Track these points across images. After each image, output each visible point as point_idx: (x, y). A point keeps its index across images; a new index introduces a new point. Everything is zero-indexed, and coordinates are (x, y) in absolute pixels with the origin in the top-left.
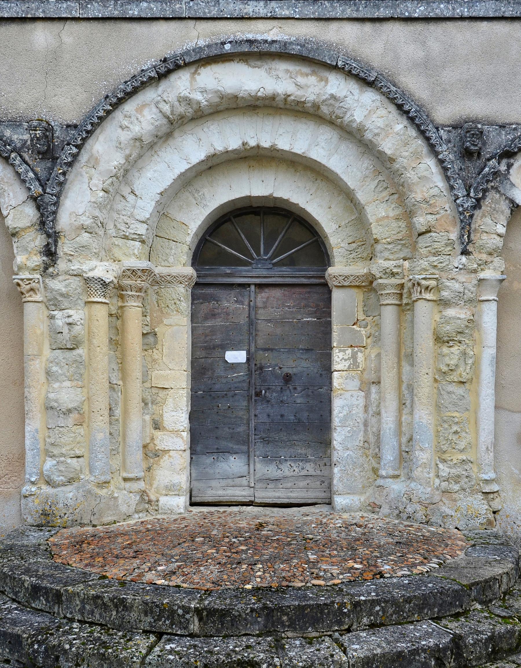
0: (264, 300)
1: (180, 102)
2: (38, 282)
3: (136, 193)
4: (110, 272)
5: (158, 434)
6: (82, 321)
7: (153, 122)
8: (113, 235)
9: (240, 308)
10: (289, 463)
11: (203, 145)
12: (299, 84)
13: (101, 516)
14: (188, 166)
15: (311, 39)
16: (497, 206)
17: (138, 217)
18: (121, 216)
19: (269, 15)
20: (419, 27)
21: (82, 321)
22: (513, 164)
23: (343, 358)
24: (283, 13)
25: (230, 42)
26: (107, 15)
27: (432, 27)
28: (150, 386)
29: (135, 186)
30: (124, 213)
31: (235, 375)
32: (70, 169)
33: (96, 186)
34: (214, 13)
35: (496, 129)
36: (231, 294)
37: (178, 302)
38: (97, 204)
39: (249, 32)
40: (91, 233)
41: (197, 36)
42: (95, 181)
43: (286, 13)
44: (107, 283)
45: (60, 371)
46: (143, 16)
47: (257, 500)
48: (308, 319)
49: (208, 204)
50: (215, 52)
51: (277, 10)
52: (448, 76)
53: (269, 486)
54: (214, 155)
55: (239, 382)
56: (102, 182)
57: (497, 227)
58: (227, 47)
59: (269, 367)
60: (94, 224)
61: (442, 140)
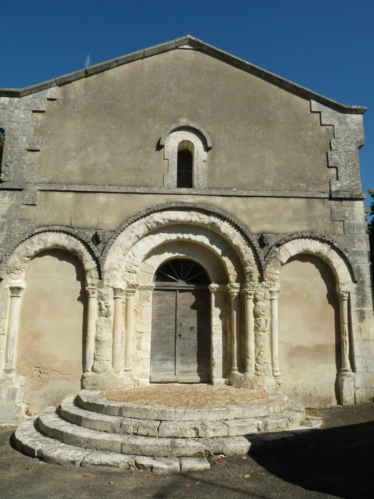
1: (154, 223)
5: (139, 352)
10: (192, 365)
13: (116, 386)
17: (135, 264)
19: (189, 193)
20: (245, 198)
22: (281, 248)
26: (127, 191)
27: (249, 199)
30: (129, 262)
34: (168, 192)
39: (181, 199)
42: (120, 251)
43: (195, 192)
46: (141, 192)
47: (179, 381)
50: (168, 206)
52: (256, 216)
53: (184, 375)
55: (172, 330)
58: (173, 204)
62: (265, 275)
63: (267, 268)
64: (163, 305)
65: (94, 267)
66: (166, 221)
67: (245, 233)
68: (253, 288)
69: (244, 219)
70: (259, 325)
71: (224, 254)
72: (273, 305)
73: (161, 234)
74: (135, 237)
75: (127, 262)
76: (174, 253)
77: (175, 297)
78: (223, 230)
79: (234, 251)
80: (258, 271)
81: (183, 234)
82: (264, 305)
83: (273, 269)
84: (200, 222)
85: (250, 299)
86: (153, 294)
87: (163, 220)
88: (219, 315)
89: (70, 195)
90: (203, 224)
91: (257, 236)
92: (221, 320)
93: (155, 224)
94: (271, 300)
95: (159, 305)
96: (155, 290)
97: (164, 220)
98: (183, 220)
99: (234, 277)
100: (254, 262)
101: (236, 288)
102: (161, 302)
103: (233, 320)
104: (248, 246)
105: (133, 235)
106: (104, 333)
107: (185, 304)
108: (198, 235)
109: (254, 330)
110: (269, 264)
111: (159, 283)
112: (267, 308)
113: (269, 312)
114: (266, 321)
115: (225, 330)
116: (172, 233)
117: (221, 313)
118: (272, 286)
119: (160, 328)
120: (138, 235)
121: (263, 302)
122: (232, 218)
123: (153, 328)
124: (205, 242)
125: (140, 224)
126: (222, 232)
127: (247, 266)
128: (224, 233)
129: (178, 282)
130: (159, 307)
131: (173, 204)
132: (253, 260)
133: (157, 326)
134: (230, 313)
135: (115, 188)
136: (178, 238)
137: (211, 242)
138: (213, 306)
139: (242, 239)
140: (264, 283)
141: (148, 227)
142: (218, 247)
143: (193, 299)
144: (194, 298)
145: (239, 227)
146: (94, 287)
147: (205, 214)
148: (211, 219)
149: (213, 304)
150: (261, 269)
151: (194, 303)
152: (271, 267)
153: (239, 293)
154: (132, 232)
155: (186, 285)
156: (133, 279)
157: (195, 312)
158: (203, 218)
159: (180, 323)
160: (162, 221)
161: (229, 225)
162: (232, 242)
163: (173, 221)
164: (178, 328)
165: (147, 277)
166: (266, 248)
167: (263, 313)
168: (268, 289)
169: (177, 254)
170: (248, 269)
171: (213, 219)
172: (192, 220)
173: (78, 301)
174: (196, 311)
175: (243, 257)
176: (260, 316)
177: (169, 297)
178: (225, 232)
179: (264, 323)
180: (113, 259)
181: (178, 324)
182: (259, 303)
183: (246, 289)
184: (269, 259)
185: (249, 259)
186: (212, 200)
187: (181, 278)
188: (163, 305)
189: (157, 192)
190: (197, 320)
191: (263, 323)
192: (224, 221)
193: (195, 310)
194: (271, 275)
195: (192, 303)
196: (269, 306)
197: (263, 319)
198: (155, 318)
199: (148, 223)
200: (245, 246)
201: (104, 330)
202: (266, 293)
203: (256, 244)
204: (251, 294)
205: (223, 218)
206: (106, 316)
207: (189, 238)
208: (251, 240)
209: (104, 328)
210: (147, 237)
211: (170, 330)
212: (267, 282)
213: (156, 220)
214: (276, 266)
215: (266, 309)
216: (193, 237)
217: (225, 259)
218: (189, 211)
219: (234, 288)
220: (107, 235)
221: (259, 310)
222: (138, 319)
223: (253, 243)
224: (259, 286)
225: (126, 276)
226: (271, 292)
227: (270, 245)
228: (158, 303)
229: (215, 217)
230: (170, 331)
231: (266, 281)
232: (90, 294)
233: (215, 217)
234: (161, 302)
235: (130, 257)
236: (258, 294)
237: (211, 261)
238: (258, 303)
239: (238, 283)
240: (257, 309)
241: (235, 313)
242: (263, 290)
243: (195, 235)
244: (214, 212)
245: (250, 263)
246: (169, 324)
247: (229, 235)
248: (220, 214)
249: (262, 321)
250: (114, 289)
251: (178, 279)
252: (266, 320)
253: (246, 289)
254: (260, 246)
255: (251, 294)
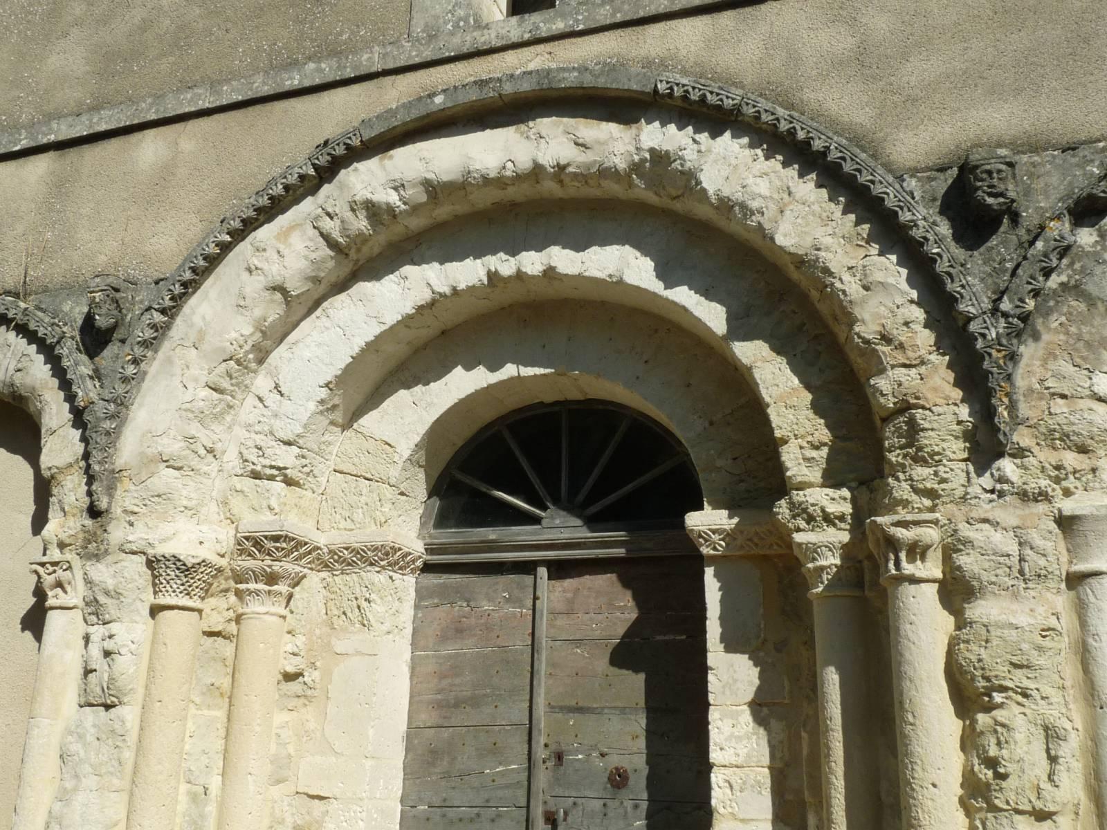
0: (569, 595)
1: (353, 210)
2: (70, 568)
3: (282, 389)
4: (206, 545)
6: (133, 647)
7: (307, 253)
8: (234, 472)
9: (514, 614)
11: (410, 286)
12: (581, 141)
14: (378, 330)
15: (609, 60)
16: (1085, 329)
18: (253, 435)
19: (527, 36)
21: (133, 647)
23: (732, 736)
24: (554, 27)
25: (444, 91)
26: (250, 95)
28: (293, 789)
29: (280, 377)
30: (257, 428)
31: (501, 769)
32: (149, 354)
33: (196, 380)
35: (1054, 157)
36: (497, 583)
37: (364, 604)
38: (193, 412)
40: (179, 469)
41: (396, 96)
42: (194, 371)
43: (559, 26)
44: (190, 565)
45: (82, 753)
48: (666, 638)
49: (435, 401)
51: (541, 25)
54: (432, 304)
55: (507, 786)
56: (206, 372)
57: (1094, 380)
58: (439, 100)
59: (577, 752)
60: (188, 452)
61: (913, 198)
62: (1012, 407)
63: (1023, 363)
64: (468, 647)
65: (71, 460)
66: (409, 193)
67: (848, 167)
68: (932, 509)
69: (839, 107)
70: (992, 763)
71: (740, 327)
72: (1093, 619)
73: (408, 270)
74: (267, 293)
75: (248, 427)
76: (493, 368)
77: (529, 603)
78: (713, 181)
79: (803, 299)
80: (958, 394)
81: (513, 253)
82: (1023, 620)
83: (1068, 369)
84: (588, 166)
85: (914, 580)
86: (421, 594)
87: (396, 189)
88: (749, 695)
89: (40, 166)
90: (606, 173)
91: (930, 179)
92: (762, 731)
93: (362, 215)
94: (1075, 580)
95: (449, 650)
96: (428, 568)
97: (398, 187)
98: (492, 175)
99: (814, 454)
100: (925, 338)
101: (828, 519)
102: (458, 630)
103: (828, 729)
104: (875, 249)
105: (254, 285)
106: (80, 798)
107: (578, 642)
108: (595, 249)
109: (962, 802)
110: (1036, 337)
111: (451, 535)
112: (1047, 643)
113: (1071, 672)
114: (1051, 734)
115: (789, 797)
116: (461, 260)
117: (759, 689)
118: (1070, 483)
119: (447, 776)
120: (278, 280)
121: (1015, 596)
122: (763, 104)
123: (410, 772)
124: (631, 278)
125: (291, 228)
126: (711, 192)
127: (882, 371)
128: (721, 199)
129: (545, 522)
130: (450, 657)
131: (439, 100)
132: (918, 327)
133: (432, 764)
134: (812, 690)
135: (200, 95)
136: (493, 276)
137: (667, 274)
138: (709, 645)
139: (837, 210)
140: (1007, 466)
141: (326, 237)
142: (708, 293)
143: (622, 609)
144: (631, 604)
145: (807, 143)
146: (69, 555)
147: (608, 120)
148: (643, 137)
149: (713, 629)
150: (975, 377)
151: (629, 634)
152: (1051, 355)
153: (847, 551)
154: (250, 271)
155: (584, 534)
156: (270, 508)
157: (634, 684)
158: (598, 142)
159: (553, 747)
160: (393, 198)
161: (747, 152)
162: (772, 239)
163: (445, 183)
164: (542, 777)
165: (363, 499)
166: (1004, 243)
167: (1019, 678)
168: (1042, 507)
169: (510, 370)
170: (887, 386)
171: (656, 135)
172: (541, 161)
173: (23, 630)
174: (641, 677)
175: (851, 320)
176: (998, 698)
177: (495, 599)
178: (726, 192)
179: (1038, 747)
180: (165, 402)
181: (541, 753)
182: (981, 610)
183: (879, 519)
184: (1031, 304)
185: (889, 323)
186: (653, 41)
187: (557, 502)
188: (468, 647)
189: (374, 69)
190: (648, 731)
191: (1023, 750)
192: (721, 133)
193: (636, 671)
194: (1059, 406)
195: (621, 630)
196: (1067, 622)
197: (1019, 723)
198: (425, 717)
199: (328, 214)
200: (862, 252)
201: (90, 782)
202: (1035, 538)
203: (935, 230)
204: (917, 551)
205: (709, 116)
206: (108, 707)
207: (550, 272)
208: (890, 202)
209: (87, 768)
210: (342, 297)
211: (501, 787)
212: (1030, 461)
213: (362, 193)
214: (1088, 345)
215: (1040, 649)
216: (564, 260)
217: (754, 355)
218: (523, 122)
219: (810, 519)
220: (141, 302)
221: (989, 658)
222: (312, 725)
223: (905, 216)
224: (975, 490)
225: (240, 497)
226: (1066, 523)
227: (1029, 216)
228: (443, 638)
229: (663, 125)
230: (500, 793)
231: (1020, 453)
232: (50, 594)
233: (663, 125)
234: (458, 630)
235: (260, 399)
236: (967, 542)
237: (689, 385)
238: (979, 610)
239: (837, 486)
240: (970, 653)
241: (832, 679)
242: (1009, 513)
243: (579, 246)
244: (656, 90)
245: (901, 346)
246: (495, 751)
247: (754, 205)
248: (685, 97)
249: (1019, 736)
250: (150, 564)
251: (544, 508)
252: (1046, 729)
253: (879, 519)
254: (958, 238)
255: (917, 551)
